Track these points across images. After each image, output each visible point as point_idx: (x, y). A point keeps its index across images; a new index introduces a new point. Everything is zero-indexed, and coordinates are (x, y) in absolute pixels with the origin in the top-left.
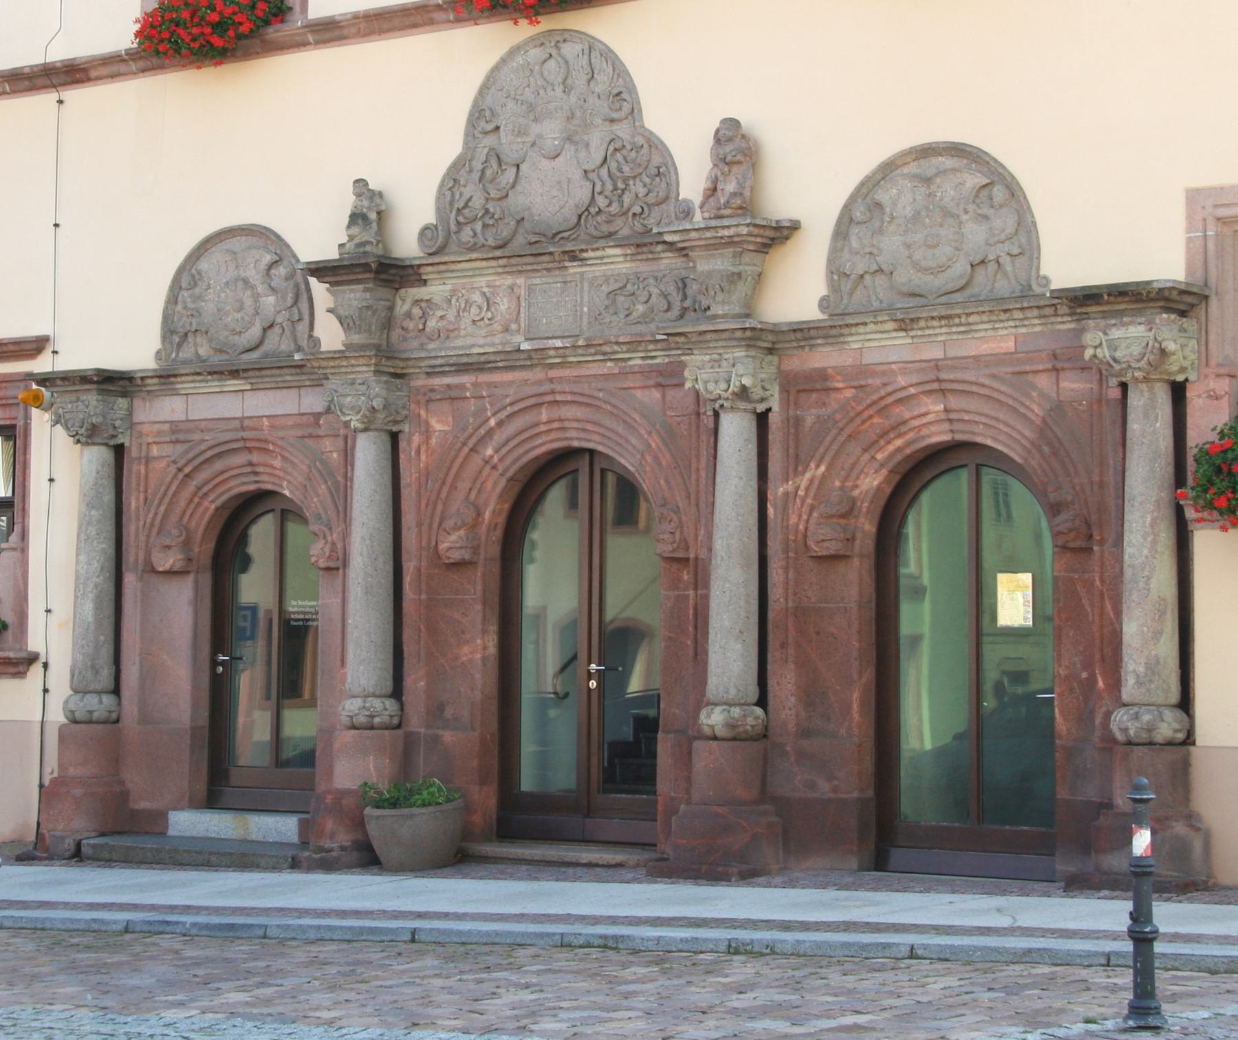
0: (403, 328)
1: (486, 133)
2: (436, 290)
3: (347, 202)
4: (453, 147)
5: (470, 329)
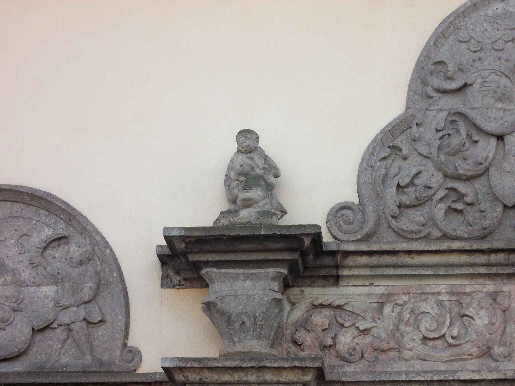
0: (295, 342)
1: (445, 92)
2: (353, 293)
3: (224, 150)
4: (392, 105)
5: (420, 349)
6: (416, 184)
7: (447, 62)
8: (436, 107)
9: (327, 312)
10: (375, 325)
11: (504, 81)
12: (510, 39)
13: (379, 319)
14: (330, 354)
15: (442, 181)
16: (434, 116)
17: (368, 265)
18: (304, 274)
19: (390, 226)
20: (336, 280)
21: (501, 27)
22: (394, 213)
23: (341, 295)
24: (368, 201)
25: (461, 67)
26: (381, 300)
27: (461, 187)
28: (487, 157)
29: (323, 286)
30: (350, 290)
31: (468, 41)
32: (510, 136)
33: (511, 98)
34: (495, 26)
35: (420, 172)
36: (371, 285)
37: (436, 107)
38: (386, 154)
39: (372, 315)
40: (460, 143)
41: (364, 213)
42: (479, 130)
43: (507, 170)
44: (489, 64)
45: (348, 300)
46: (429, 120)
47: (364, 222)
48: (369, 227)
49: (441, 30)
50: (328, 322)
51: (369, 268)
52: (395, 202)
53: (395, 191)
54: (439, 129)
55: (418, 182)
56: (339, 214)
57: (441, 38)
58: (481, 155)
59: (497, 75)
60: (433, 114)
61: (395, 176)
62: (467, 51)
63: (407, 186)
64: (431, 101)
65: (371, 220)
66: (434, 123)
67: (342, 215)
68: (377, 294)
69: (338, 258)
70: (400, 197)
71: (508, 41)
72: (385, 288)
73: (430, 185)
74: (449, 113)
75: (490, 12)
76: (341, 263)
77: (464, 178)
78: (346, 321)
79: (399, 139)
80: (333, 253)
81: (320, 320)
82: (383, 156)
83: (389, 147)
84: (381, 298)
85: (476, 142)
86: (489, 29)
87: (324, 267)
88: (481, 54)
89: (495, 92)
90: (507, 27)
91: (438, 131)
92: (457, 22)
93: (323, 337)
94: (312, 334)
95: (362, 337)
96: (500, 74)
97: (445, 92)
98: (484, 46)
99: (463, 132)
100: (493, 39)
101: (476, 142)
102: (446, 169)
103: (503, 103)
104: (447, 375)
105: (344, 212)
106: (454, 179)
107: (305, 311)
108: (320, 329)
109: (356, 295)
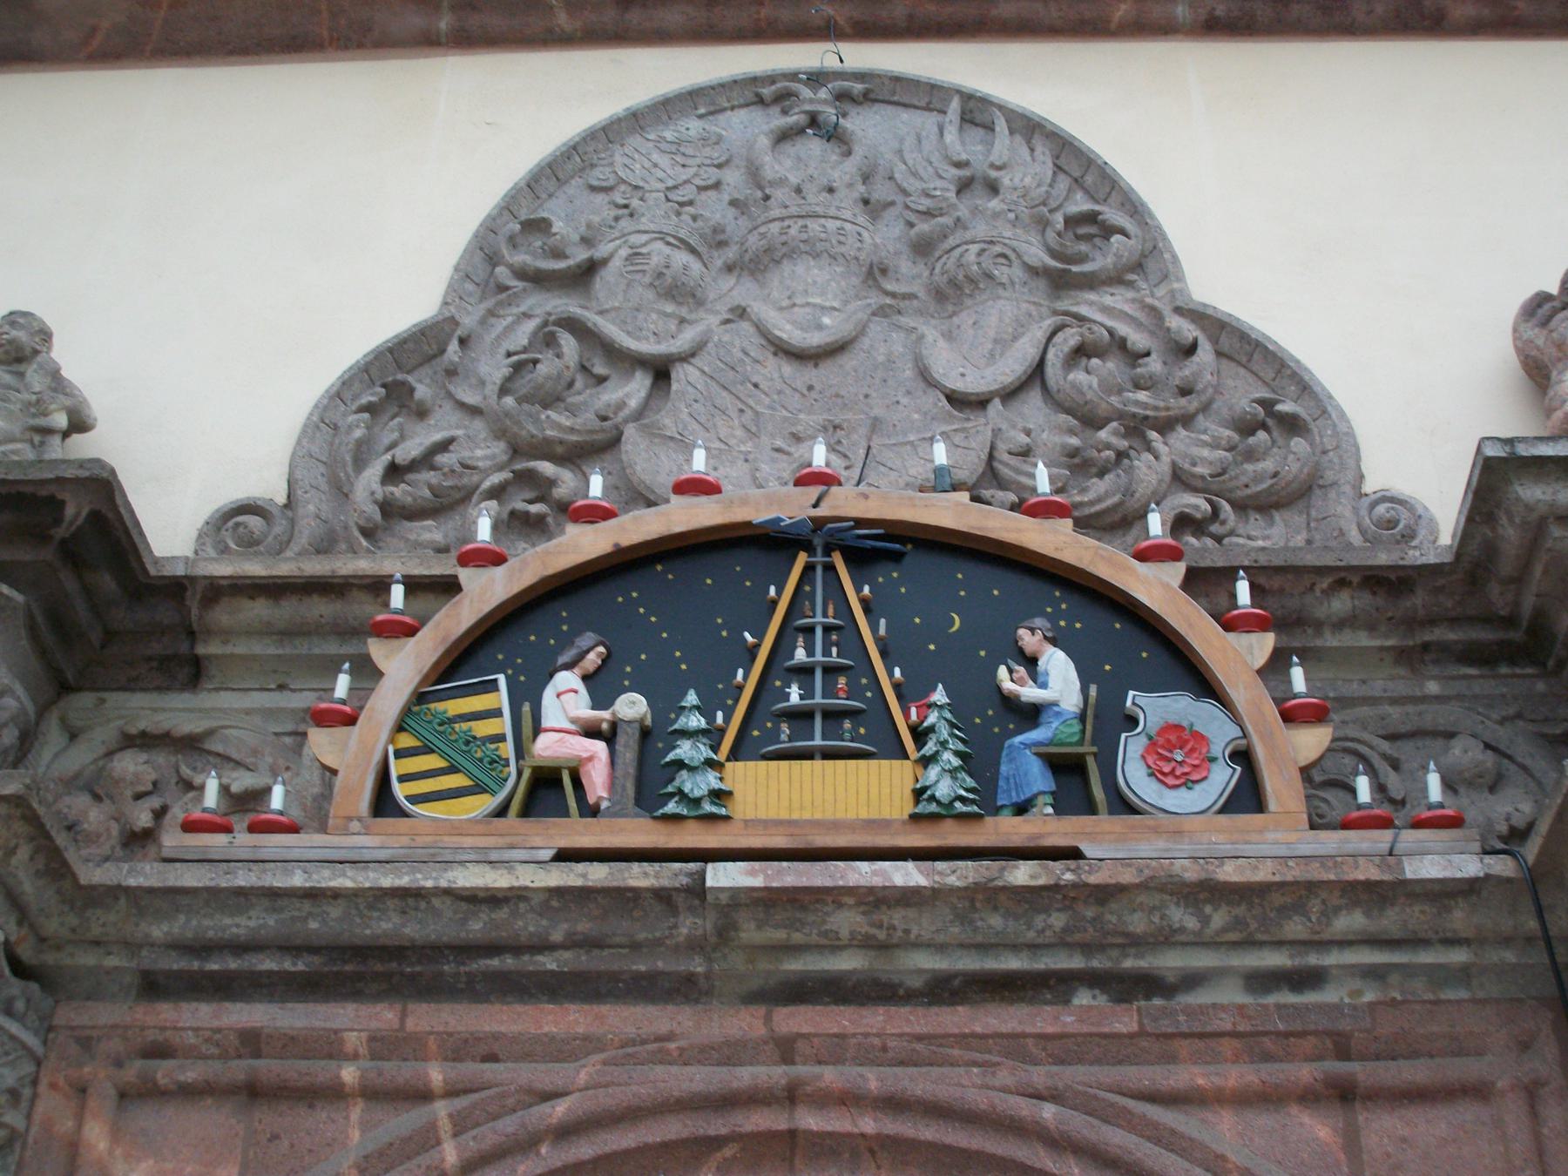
4: (410, 297)
9: (162, 758)
11: (681, 258)
12: (710, 182)
13: (288, 769)
20: (191, 672)
21: (689, 162)
22: (368, 520)
23: (200, 710)
30: (227, 700)
33: (698, 294)
34: (679, 158)
35: (451, 441)
36: (281, 687)
37: (515, 310)
41: (292, 522)
50: (153, 776)
56: (230, 524)
59: (668, 244)
67: (238, 525)
68: (293, 710)
77: (560, 450)
80: (176, 588)
83: (384, 386)
90: (708, 162)
91: (509, 355)
94: (107, 806)
100: (670, 183)
101: (601, 380)
102: (515, 429)
103: (681, 304)
104: (419, 876)
108: (129, 793)
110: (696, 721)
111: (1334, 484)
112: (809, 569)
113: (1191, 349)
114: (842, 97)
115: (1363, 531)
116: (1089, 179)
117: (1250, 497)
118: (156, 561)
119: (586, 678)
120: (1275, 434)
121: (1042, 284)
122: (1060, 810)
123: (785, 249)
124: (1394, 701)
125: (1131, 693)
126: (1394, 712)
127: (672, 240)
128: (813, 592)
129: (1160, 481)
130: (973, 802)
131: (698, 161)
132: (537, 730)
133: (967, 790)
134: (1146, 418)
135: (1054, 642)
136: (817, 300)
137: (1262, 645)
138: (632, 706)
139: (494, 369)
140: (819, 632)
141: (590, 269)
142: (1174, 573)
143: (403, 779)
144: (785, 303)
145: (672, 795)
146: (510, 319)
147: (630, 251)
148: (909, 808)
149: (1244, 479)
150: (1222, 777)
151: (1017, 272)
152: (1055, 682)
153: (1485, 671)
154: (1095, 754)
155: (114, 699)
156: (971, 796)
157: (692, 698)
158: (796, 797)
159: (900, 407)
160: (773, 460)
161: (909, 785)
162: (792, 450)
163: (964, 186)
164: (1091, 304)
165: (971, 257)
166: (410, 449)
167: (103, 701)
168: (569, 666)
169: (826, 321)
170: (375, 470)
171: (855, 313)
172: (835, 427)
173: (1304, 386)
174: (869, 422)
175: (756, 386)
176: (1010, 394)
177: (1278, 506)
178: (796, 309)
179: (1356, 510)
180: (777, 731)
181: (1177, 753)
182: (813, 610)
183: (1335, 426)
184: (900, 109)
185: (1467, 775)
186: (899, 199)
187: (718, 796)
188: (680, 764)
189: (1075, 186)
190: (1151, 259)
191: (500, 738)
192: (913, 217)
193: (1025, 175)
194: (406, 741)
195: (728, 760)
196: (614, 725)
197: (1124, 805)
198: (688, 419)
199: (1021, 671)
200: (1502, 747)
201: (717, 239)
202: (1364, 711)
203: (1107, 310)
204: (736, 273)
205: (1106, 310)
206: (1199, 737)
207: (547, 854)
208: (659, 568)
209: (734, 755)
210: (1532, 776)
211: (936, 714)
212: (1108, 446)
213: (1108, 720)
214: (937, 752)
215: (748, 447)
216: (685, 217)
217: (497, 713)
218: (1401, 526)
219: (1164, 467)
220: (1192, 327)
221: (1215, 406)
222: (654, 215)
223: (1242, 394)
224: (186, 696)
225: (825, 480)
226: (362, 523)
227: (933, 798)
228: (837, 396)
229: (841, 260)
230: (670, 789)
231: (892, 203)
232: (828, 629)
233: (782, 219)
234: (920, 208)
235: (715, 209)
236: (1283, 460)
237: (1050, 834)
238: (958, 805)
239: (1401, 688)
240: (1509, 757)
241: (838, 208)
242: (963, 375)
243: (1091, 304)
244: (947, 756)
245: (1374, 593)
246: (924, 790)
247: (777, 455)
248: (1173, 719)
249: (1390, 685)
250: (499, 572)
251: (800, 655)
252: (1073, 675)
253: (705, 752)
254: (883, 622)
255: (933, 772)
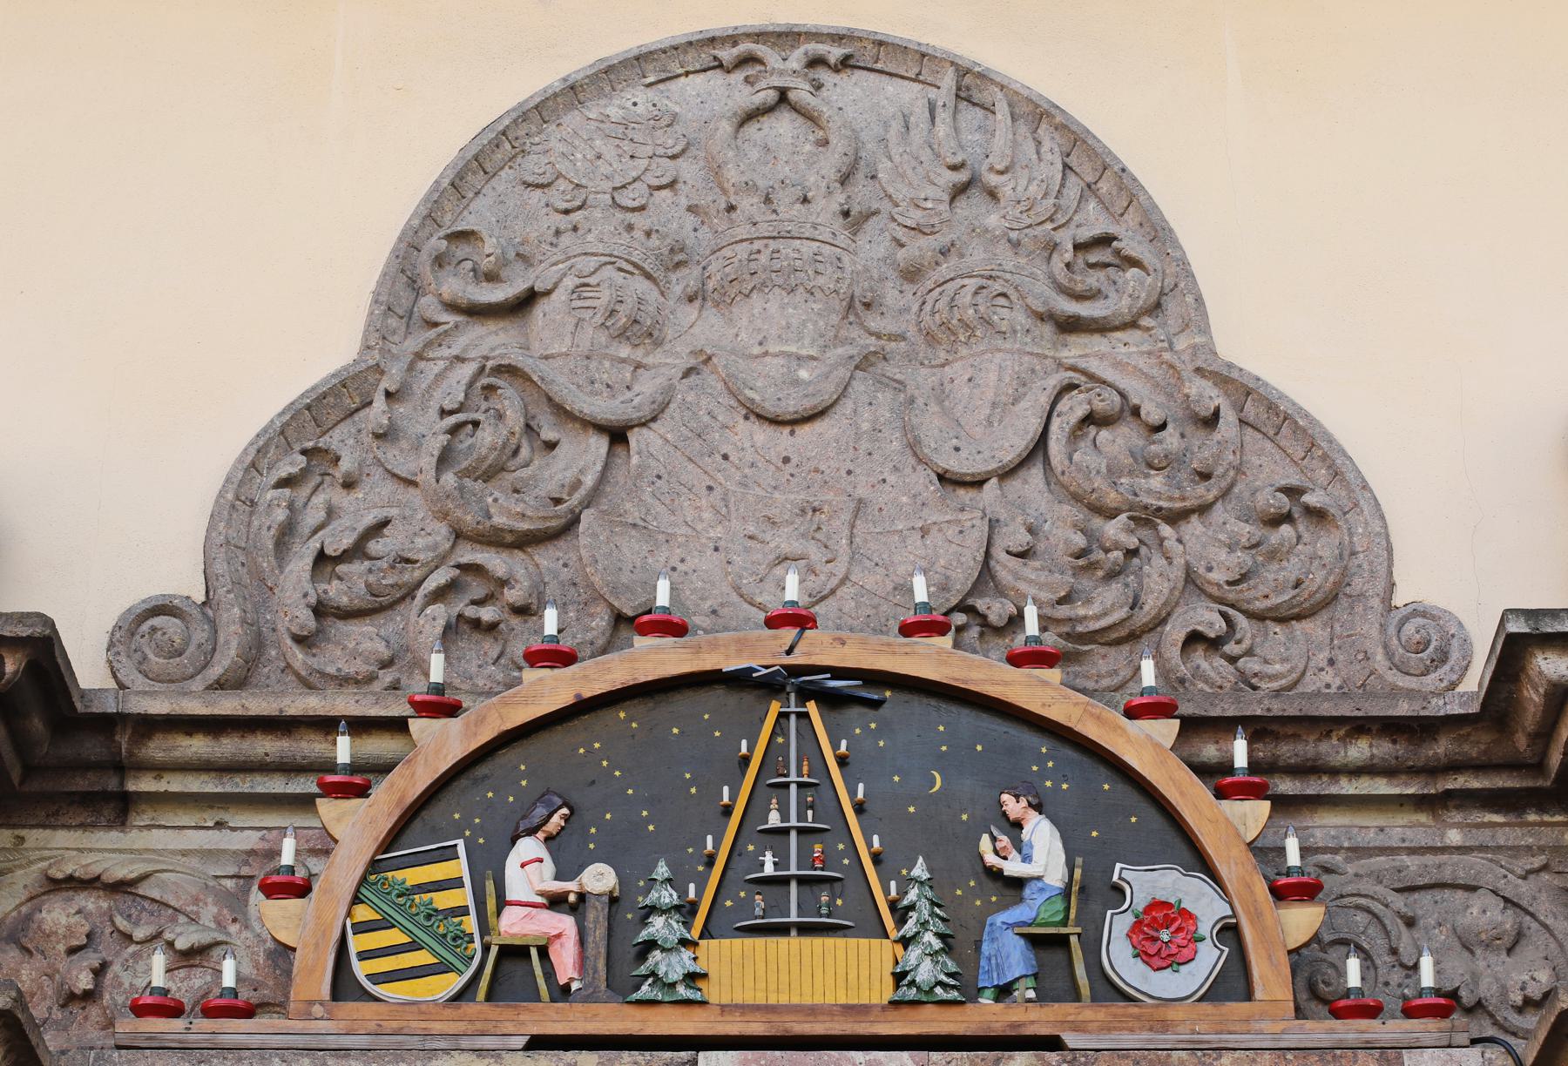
1: (476, 312)
2: (165, 848)
6: (374, 554)
7: (484, 234)
8: (446, 352)
9: (91, 902)
10: (221, 937)
11: (640, 285)
12: (664, 181)
13: (235, 920)
14: (86, 1018)
15: (448, 545)
16: (440, 377)
17: (208, 761)
18: (26, 789)
19: (288, 666)
20: (120, 808)
23: (132, 851)
24: (229, 592)
25: (521, 250)
26: (245, 871)
27: (496, 562)
28: (577, 484)
29: (83, 826)
30: (158, 839)
31: (549, 185)
32: (644, 431)
35: (385, 523)
36: (219, 825)
37: (446, 352)
38: (294, 470)
39: (215, 910)
40: (504, 446)
41: (214, 625)
42: (563, 413)
43: (630, 521)
44: (601, 241)
45: (150, 868)
46: (424, 386)
47: (214, 650)
48: (226, 663)
49: (474, 150)
50: (87, 928)
51: (213, 774)
52: (305, 595)
53: (309, 568)
54: (448, 407)
55: (379, 547)
56: (145, 627)
57: (474, 173)
58: (560, 476)
59: (620, 269)
60: (436, 370)
61: (315, 532)
62: (545, 210)
63: (346, 556)
64: (432, 333)
65: (234, 644)
66: (437, 394)
67: (154, 629)
69: (123, 740)
70: (322, 586)
71: (659, 188)
72: (260, 834)
73: (409, 555)
74: (483, 368)
75: (614, 112)
76: (131, 754)
77: (509, 538)
78: (137, 924)
79: (337, 433)
80: (108, 723)
81: (64, 921)
82: (284, 475)
83: (304, 452)
84: (246, 863)
85: (551, 446)
86: (609, 151)
87: (85, 767)
88: (577, 217)
89: (613, 312)
91: (444, 413)
92: (521, 133)
93: (69, 971)
95: (182, 973)
96: (630, 268)
97: (476, 312)
98: (592, 196)
99: (514, 419)
101: (551, 446)
102: (459, 513)
105: (157, 621)
106: (481, 543)
107: (24, 898)
108: (61, 947)
109: (174, 852)
110: (667, 896)
111: (1362, 595)
112: (783, 716)
113: (1211, 421)
114: (816, 62)
115: (1389, 655)
116: (1104, 187)
117: (1270, 609)
118: (83, 694)
119: (549, 839)
120: (1301, 528)
121: (1047, 330)
122: (1043, 997)
123: (756, 280)
124: (1412, 851)
125: (1118, 866)
126: (1412, 862)
127: (625, 265)
128: (787, 744)
129: (1172, 590)
130: (953, 987)
131: (649, 150)
132: (502, 903)
133: (949, 975)
134: (1160, 509)
135: (1038, 808)
136: (793, 349)
137: (1253, 814)
138: (599, 878)
139: (431, 431)
140: (793, 788)
141: (527, 301)
142: (1166, 730)
143: (364, 956)
144: (757, 350)
145: (646, 977)
146: (441, 364)
147: (578, 281)
148: (889, 994)
149: (1263, 589)
150: (1209, 958)
151: (1021, 319)
152: (1039, 854)
153: (1512, 818)
154: (1079, 935)
155: (34, 837)
156: (952, 982)
157: (662, 871)
158: (772, 978)
159: (887, 487)
160: (747, 550)
161: (889, 967)
162: (768, 537)
163: (959, 191)
164: (1102, 357)
165: (966, 298)
166: (338, 540)
167: (22, 839)
168: (531, 832)
169: (804, 374)
170: (301, 562)
171: (835, 367)
172: (814, 510)
173: (1338, 467)
174: (853, 505)
175: (725, 457)
176: (1007, 473)
177: (1305, 617)
178: (768, 359)
179: (1383, 628)
180: (750, 901)
181: (1162, 933)
182: (787, 766)
183: (1367, 523)
184: (885, 78)
185: (1483, 937)
186: (886, 206)
187: (692, 978)
188: (651, 945)
189: (1087, 192)
190: (1170, 299)
191: (463, 911)
192: (900, 233)
193: (1030, 181)
194: (363, 913)
195: (701, 937)
196: (582, 896)
197: (1110, 990)
198: (650, 500)
199: (1004, 841)
200: (1524, 903)
201: (677, 258)
202: (1380, 861)
203: (1121, 363)
204: (697, 303)
205: (1118, 365)
206: (1186, 915)
207: (521, 1042)
208: (622, 715)
209: (706, 933)
210: (1552, 935)
211: (916, 890)
212: (1117, 546)
213: (1092, 891)
214: (918, 933)
215: (718, 532)
216: (638, 234)
217: (457, 883)
218: (1433, 644)
219: (1177, 573)
220: (1214, 392)
221: (1236, 490)
222: (602, 229)
223: (1269, 471)
224: (114, 834)
225: (800, 620)
226: (295, 629)
227: (912, 983)
228: (816, 470)
229: (818, 294)
230: (643, 970)
231: (876, 213)
232: (800, 785)
233: (751, 240)
234: (909, 223)
235: (669, 213)
236: (1307, 558)
237: (1033, 1022)
238: (938, 990)
239: (1421, 838)
240: (1532, 915)
241: (815, 226)
242: (957, 449)
243: (1102, 357)
244: (928, 937)
245: (1394, 742)
246: (904, 974)
247: (750, 543)
248: (1161, 896)
249: (1409, 833)
250: (453, 725)
251: (774, 820)
252: (1058, 845)
253: (679, 930)
254: (861, 787)
255: (914, 953)
